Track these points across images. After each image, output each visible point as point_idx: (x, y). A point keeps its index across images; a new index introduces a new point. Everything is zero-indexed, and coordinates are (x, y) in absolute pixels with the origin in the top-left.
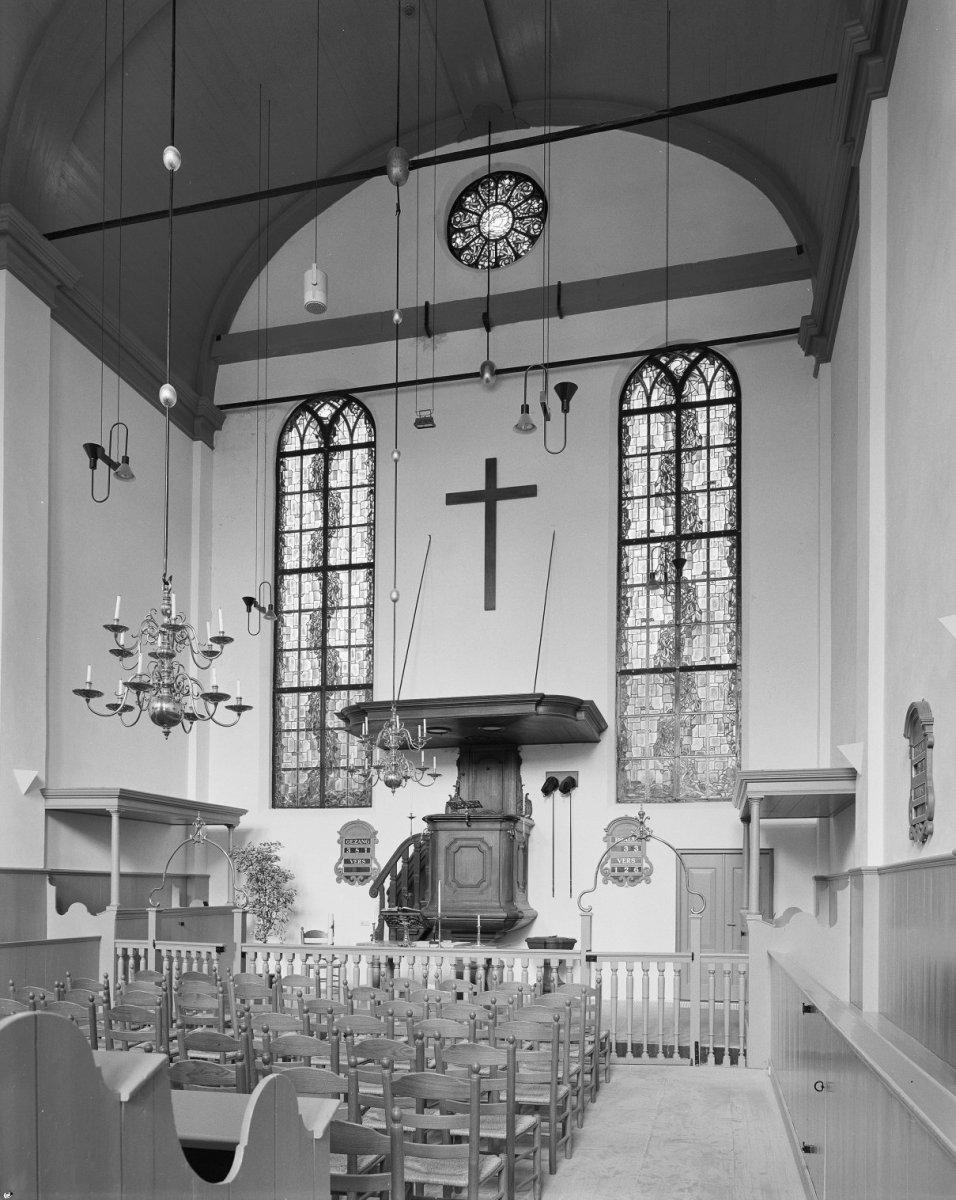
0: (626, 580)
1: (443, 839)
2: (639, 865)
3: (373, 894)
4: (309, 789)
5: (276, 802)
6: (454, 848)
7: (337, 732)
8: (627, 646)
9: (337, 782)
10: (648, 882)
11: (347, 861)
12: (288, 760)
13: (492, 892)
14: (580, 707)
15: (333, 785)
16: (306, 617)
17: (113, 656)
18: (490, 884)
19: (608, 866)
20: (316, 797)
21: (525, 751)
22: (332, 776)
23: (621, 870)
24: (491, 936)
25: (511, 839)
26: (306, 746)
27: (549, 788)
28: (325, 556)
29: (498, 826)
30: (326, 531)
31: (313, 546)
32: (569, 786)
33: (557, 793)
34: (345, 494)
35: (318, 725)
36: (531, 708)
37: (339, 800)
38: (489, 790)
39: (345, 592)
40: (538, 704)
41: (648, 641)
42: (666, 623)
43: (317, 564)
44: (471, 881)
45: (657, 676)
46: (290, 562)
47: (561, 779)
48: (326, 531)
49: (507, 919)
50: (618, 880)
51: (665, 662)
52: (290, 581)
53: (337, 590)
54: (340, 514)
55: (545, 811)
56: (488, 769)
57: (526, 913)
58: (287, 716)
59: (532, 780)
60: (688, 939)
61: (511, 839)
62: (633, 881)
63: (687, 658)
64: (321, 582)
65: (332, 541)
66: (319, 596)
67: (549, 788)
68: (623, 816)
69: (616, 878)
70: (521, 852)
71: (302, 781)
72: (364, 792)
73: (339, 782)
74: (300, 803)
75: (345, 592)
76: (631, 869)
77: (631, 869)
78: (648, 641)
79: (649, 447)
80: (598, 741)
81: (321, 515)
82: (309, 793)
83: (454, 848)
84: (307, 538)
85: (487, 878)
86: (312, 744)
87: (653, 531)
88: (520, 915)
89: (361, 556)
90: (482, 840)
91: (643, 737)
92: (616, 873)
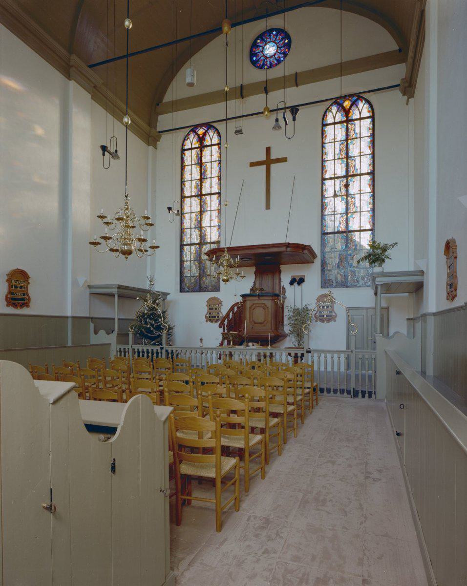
1: (248, 304)
3: (220, 327)
5: (182, 290)
6: (253, 307)
10: (335, 321)
25: (276, 304)
28: (201, 190)
29: (271, 298)
32: (301, 281)
33: (296, 284)
35: (199, 258)
38: (267, 284)
45: (339, 234)
46: (187, 193)
47: (297, 279)
48: (201, 180)
52: (187, 201)
65: (204, 184)
83: (253, 307)
90: (264, 304)
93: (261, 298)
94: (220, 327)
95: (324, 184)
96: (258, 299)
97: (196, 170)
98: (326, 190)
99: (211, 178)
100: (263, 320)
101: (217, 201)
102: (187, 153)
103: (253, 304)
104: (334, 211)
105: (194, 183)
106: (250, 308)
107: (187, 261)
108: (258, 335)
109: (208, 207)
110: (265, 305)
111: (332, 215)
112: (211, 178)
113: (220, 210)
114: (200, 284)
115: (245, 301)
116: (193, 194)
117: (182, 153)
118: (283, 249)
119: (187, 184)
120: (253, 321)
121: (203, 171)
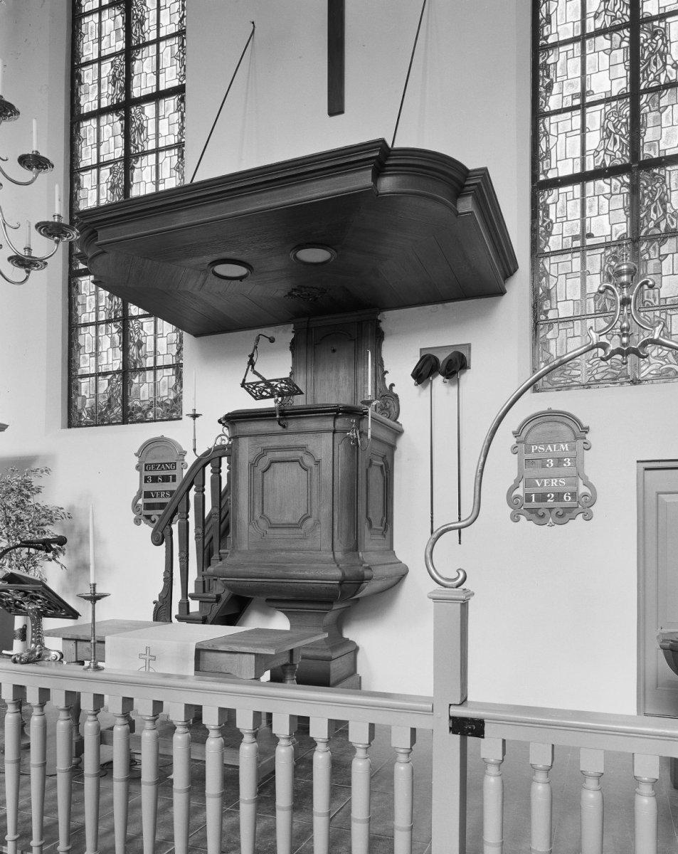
0: (546, 38)
1: (246, 450)
2: (573, 489)
3: (157, 541)
4: (109, 400)
5: (72, 420)
6: (264, 463)
8: (548, 141)
9: (142, 389)
10: (588, 517)
11: (148, 495)
12: (86, 364)
13: (321, 538)
14: (463, 186)
15: (137, 392)
16: (105, 172)
18: (318, 522)
19: (520, 492)
20: (118, 410)
21: (389, 319)
22: (136, 381)
23: (542, 498)
25: (354, 449)
26: (106, 343)
27: (425, 371)
28: (127, 88)
29: (329, 424)
30: (129, 54)
31: (114, 76)
32: (455, 366)
33: (439, 380)
35: (120, 314)
36: (363, 179)
38: (331, 386)
39: (151, 130)
40: (379, 171)
41: (583, 128)
42: (615, 93)
43: (118, 100)
44: (288, 518)
45: (600, 182)
46: (88, 103)
47: (442, 357)
48: (129, 54)
50: (538, 516)
51: (613, 158)
52: (88, 127)
53: (141, 129)
54: (145, 27)
55: (417, 407)
57: (382, 572)
58: (84, 305)
59: (399, 361)
60: (203, 559)
62: (561, 516)
63: (652, 145)
64: (123, 122)
65: (136, 65)
66: (121, 141)
67: (425, 371)
68: (545, 409)
69: (532, 511)
70: (376, 475)
71: (101, 390)
73: (143, 389)
74: (100, 419)
75: (151, 130)
76: (559, 496)
77: (559, 496)
78: (583, 128)
79: (583, 94)
80: (501, 292)
81: (122, 33)
82: (109, 406)
83: (264, 463)
84: (107, 67)
86: (112, 339)
87: (590, 236)
88: (367, 573)
89: (169, 80)
90: (303, 448)
91: (572, 285)
92: (534, 504)
93: (293, 425)
94: (157, 541)
96: (279, 428)
100: (302, 512)
103: (266, 450)
106: (253, 465)
107: (86, 325)
109: (147, 140)
110: (308, 453)
111: (575, 250)
114: (125, 398)
115: (234, 437)
116: (105, 103)
118: (363, 179)
119: (88, 75)
120: (263, 516)
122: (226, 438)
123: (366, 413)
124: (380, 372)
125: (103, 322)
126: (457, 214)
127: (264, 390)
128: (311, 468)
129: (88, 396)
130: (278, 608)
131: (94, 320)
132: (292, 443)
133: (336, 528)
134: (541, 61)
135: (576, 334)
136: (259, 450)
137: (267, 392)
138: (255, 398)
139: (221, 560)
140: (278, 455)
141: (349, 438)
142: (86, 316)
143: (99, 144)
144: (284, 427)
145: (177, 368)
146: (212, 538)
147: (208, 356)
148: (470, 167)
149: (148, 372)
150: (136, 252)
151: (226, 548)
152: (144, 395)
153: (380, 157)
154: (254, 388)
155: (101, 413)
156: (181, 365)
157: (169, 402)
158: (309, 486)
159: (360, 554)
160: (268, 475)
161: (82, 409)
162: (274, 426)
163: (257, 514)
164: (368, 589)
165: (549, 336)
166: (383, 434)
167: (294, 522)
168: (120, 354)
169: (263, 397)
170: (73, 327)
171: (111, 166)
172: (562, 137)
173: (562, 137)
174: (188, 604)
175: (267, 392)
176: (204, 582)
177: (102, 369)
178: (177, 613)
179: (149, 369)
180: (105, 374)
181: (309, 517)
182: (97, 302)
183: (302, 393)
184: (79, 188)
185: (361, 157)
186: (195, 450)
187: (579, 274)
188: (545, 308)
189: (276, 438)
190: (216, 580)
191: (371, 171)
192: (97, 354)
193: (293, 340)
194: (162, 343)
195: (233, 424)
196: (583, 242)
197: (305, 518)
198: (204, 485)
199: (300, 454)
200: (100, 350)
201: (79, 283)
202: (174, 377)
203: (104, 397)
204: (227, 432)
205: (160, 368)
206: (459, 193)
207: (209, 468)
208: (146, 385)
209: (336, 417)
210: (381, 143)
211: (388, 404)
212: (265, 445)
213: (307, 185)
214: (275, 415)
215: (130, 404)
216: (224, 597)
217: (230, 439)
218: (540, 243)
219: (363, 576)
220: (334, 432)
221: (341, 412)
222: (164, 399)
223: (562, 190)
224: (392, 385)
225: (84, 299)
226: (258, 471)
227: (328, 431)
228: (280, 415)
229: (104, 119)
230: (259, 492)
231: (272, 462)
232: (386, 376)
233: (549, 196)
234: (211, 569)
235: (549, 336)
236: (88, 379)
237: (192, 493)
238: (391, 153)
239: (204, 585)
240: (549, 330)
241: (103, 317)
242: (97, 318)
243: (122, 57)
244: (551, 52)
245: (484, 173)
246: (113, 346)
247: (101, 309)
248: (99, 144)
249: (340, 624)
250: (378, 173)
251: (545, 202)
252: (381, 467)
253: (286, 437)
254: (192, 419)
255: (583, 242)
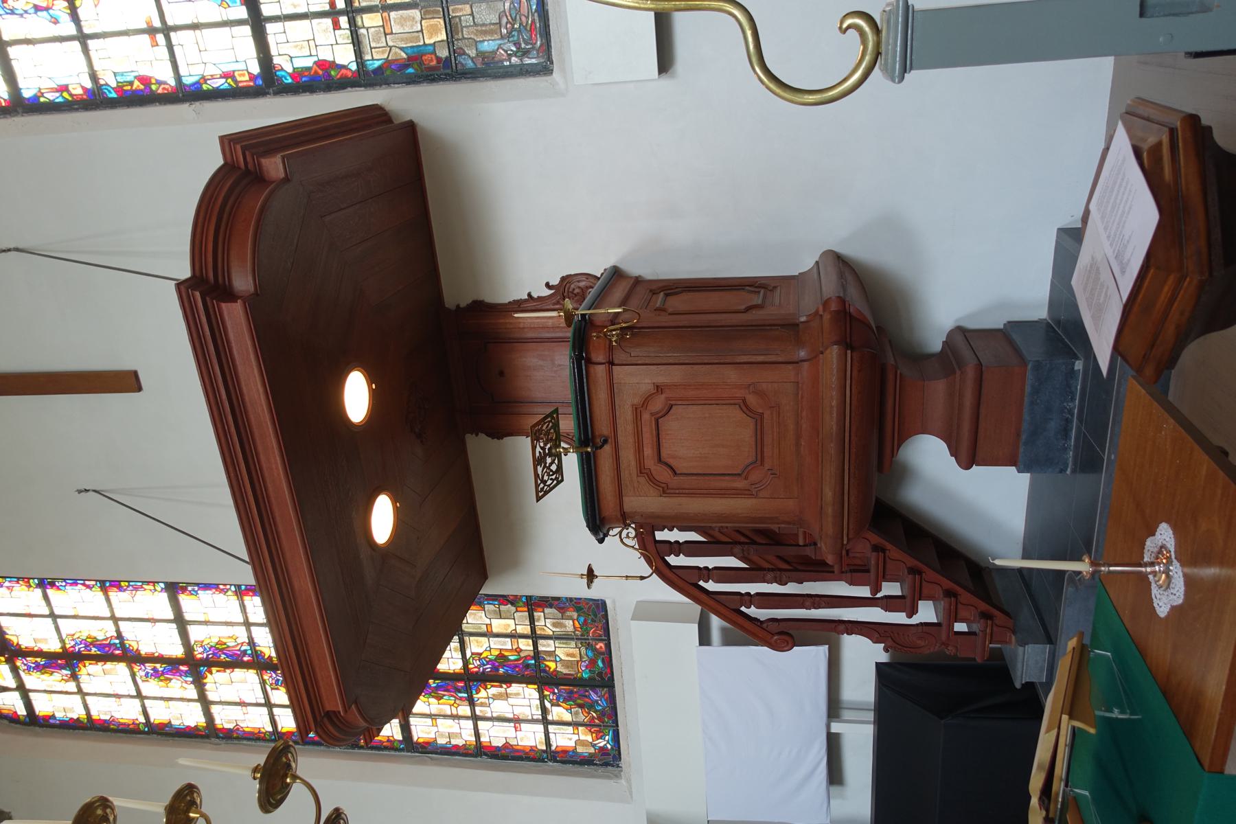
1: (643, 501)
6: (663, 474)
7: (468, 655)
8: (213, 77)
12: (531, 737)
14: (247, 172)
15: (566, 664)
17: (594, 585)
21: (455, 295)
22: (552, 665)
24: (891, 377)
25: (633, 333)
26: (500, 708)
29: (600, 371)
30: (131, 658)
34: (66, 626)
37: (598, 653)
38: (548, 375)
41: (195, 27)
46: (192, 716)
48: (131, 658)
49: (847, 344)
52: (224, 718)
56: (502, 374)
57: (830, 288)
61: (633, 333)
64: (214, 670)
65: (145, 650)
70: (676, 303)
71: (567, 717)
72: (578, 610)
73: (563, 656)
82: (587, 706)
83: (663, 474)
85: (740, 393)
86: (495, 697)
88: (834, 307)
90: (637, 411)
93: (602, 426)
95: (36, 98)
97: (95, 676)
98: (64, 88)
99: (115, 619)
100: (736, 413)
101: (205, 595)
102: (43, 706)
104: (151, 31)
105: (151, 687)
106: (665, 490)
107: (477, 734)
108: (832, 448)
109: (519, 651)
111: (352, 23)
112: (115, 619)
113: (239, 586)
115: (624, 519)
116: (192, 692)
117: (42, 726)
118: (234, 315)
119: (159, 713)
120: (743, 474)
121: (94, 651)
122: (625, 533)
123: (583, 316)
124: (531, 303)
125: (473, 711)
126: (287, 180)
127: (549, 468)
128: (668, 399)
129: (576, 737)
130: (894, 453)
131: (470, 722)
132: (630, 428)
133: (760, 358)
134: (114, 95)
135: (469, 11)
136: (642, 480)
137: (551, 464)
138: (559, 483)
139: (815, 544)
140: (648, 451)
141: (621, 338)
142: (464, 734)
143: (242, 704)
144: (605, 441)
145: (533, 604)
146: (779, 557)
147: (513, 562)
148: (220, 162)
149: (541, 648)
150: (359, 652)
151: (797, 535)
152: (572, 655)
153: (203, 293)
154: (544, 482)
155: (599, 718)
156: (529, 598)
157: (582, 619)
158: (694, 402)
159: (803, 319)
160: (681, 466)
161: (594, 746)
162: (605, 456)
163: (740, 484)
164: (857, 304)
165: (473, 53)
166: (619, 293)
167: (752, 426)
168: (515, 688)
169: (560, 469)
170: (481, 752)
171: (268, 688)
172: (206, 57)
173: (206, 57)
174: (886, 597)
175: (551, 464)
176: (851, 571)
177: (537, 714)
178: (904, 614)
179: (535, 645)
180: (544, 711)
181: (744, 401)
182: (445, 716)
183: (556, 411)
184: (53, 716)
185: (204, 319)
186: (642, 578)
187: (385, 14)
188: (434, 63)
189: (622, 453)
190: (847, 552)
191: (223, 305)
192: (517, 721)
193: (489, 435)
194: (498, 625)
195: (603, 521)
196: (341, 13)
197: (745, 406)
198: (698, 568)
199: (646, 416)
200: (511, 716)
201: (421, 740)
202: (547, 610)
203: (577, 713)
204: (616, 530)
205: (533, 629)
206: (257, 178)
207: (673, 560)
208: (558, 652)
209: (589, 361)
210: (182, 287)
211: (577, 291)
212: (634, 471)
213: (247, 398)
214: (588, 453)
215: (586, 676)
216: (875, 539)
217: (627, 526)
218: (346, 77)
219: (837, 312)
220: (611, 363)
221: (581, 353)
222: (577, 624)
223: (273, 51)
224: (547, 285)
225: (442, 735)
226: (676, 481)
227: (610, 374)
228: (587, 446)
229: (211, 696)
230: (705, 482)
231: (660, 460)
232: (535, 295)
233: (282, 69)
234: (830, 559)
235: (473, 53)
236: (552, 736)
237: (711, 586)
238: (198, 273)
239: (855, 573)
240: (464, 53)
241: (465, 710)
242: (466, 718)
243: (136, 668)
244: (102, 82)
245: (228, 142)
246: (506, 696)
247: (455, 712)
248: (242, 704)
249: (919, 358)
250: (228, 294)
251: (292, 75)
252: (667, 295)
253: (621, 439)
254: (595, 580)
255: (341, 13)
